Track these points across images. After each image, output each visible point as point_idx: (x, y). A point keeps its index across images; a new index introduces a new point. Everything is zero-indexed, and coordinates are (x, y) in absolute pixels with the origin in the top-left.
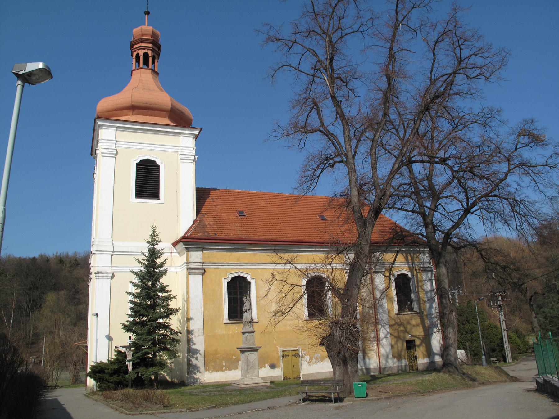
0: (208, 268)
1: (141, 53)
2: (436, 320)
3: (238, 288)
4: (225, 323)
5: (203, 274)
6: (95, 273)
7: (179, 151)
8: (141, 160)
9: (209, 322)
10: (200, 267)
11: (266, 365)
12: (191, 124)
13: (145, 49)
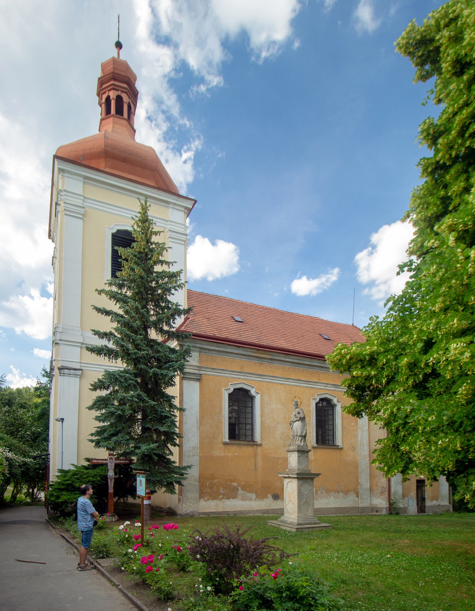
1: (113, 95)
3: (241, 399)
4: (225, 444)
5: (199, 380)
6: (59, 369)
7: (166, 226)
9: (206, 441)
11: (269, 495)
13: (118, 90)
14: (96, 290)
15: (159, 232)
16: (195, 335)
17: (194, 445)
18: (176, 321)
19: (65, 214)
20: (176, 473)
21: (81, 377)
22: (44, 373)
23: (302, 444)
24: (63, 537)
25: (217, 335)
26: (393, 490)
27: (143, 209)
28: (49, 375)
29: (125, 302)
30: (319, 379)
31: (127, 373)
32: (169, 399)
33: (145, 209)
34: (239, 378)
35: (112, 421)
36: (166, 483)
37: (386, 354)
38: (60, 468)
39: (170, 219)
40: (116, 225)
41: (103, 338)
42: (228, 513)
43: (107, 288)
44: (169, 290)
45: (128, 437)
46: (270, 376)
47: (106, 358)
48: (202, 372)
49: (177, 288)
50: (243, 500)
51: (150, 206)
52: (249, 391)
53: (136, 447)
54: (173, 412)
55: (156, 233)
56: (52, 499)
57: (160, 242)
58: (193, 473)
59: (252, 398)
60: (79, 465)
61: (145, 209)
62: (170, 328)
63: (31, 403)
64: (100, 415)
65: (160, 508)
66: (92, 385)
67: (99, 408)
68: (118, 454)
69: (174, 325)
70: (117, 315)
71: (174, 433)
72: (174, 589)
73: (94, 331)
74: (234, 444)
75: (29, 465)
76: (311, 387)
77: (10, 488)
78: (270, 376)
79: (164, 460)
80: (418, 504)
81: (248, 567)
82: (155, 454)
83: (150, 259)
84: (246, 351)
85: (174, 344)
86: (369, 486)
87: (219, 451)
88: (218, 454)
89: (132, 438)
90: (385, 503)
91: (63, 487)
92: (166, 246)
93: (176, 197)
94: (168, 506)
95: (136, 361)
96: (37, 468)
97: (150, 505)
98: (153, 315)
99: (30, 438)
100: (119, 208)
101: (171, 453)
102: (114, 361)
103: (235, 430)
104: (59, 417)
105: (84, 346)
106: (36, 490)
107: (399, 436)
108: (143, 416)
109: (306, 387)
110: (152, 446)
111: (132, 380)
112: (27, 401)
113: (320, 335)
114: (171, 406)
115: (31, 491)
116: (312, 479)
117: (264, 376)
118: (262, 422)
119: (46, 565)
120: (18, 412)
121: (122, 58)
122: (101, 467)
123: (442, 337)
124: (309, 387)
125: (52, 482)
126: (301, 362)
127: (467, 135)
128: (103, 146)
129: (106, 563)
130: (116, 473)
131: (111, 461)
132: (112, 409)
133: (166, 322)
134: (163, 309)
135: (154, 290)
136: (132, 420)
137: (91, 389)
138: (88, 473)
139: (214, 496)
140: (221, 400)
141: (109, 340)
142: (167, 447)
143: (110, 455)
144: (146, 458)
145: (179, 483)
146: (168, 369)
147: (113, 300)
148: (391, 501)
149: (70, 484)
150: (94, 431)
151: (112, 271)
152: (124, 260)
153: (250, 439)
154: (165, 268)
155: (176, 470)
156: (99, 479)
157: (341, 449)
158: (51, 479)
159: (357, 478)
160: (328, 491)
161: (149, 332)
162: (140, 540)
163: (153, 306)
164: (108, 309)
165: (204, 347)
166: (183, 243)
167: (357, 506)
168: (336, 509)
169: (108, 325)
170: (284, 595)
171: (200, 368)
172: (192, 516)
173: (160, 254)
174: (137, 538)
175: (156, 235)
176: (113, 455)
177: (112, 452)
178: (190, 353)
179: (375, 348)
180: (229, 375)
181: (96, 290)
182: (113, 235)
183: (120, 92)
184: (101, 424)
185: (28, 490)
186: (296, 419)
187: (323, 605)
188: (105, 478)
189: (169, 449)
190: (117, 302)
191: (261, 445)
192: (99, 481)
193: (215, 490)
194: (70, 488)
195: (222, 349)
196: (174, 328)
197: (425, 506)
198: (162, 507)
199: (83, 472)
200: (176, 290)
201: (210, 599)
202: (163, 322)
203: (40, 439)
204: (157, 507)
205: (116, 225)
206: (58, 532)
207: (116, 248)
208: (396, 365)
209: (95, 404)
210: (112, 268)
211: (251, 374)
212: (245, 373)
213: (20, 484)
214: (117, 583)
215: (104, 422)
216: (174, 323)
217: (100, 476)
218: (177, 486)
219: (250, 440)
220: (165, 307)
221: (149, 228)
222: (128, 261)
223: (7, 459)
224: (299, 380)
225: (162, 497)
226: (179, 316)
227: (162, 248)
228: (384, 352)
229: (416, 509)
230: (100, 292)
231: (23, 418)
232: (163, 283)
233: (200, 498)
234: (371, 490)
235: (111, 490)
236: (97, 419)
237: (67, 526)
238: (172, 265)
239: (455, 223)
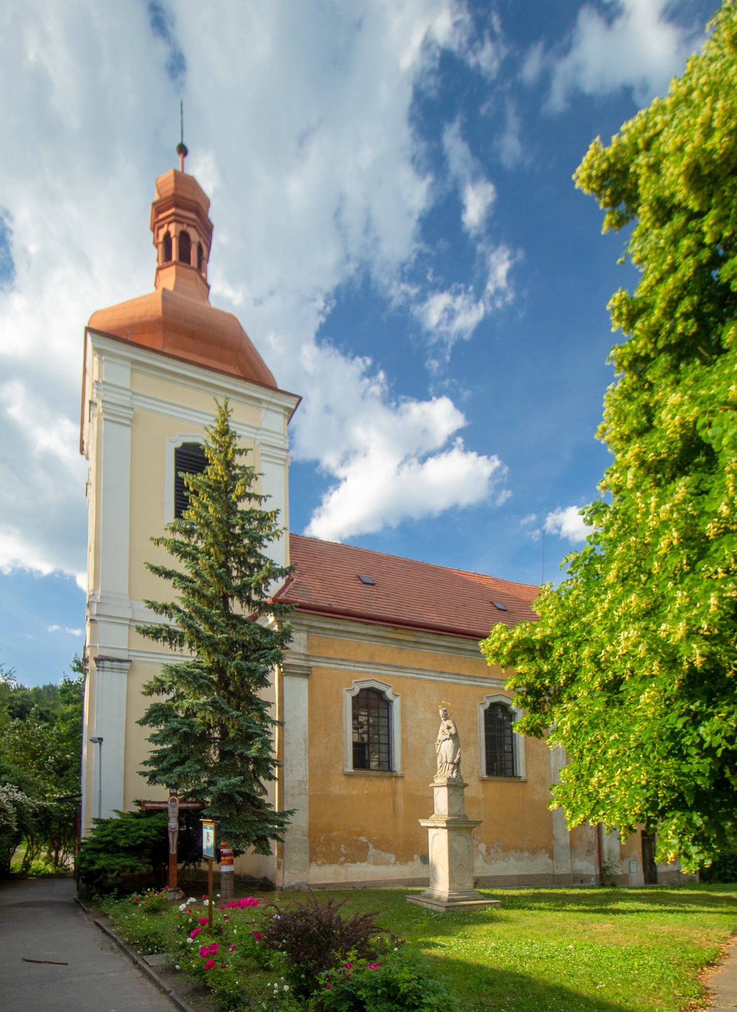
0: (317, 667)
3: (372, 704)
4: (348, 775)
5: (307, 676)
6: (97, 660)
7: (257, 437)
9: (319, 771)
11: (416, 857)
13: (182, 223)
14: (152, 539)
15: (246, 450)
16: (302, 607)
17: (300, 778)
18: (269, 588)
19: (105, 419)
20: (273, 822)
22: (75, 665)
23: (454, 775)
24: (98, 925)
25: (335, 606)
26: (605, 847)
27: (223, 415)
28: (81, 667)
29: (195, 559)
30: (489, 674)
31: (198, 667)
32: (260, 706)
33: (225, 415)
34: (368, 673)
35: (175, 742)
36: (255, 838)
37: (565, 639)
38: (97, 817)
39: (264, 426)
40: (182, 436)
41: (161, 613)
42: (352, 884)
43: (169, 535)
44: (259, 540)
45: (199, 767)
46: (414, 669)
47: (167, 644)
48: (312, 664)
49: (271, 537)
50: (376, 864)
51: (232, 410)
52: (384, 692)
53: (211, 783)
54: (267, 727)
55: (241, 452)
56: (83, 865)
57: (247, 466)
58: (299, 822)
59: (388, 703)
60: (126, 812)
61: (225, 415)
62: (262, 597)
63: (56, 712)
64: (157, 732)
65: (251, 878)
66: (145, 686)
67: (156, 723)
68: (185, 793)
69: (267, 594)
70: (182, 578)
71: (269, 760)
72: (243, 992)
73: (148, 602)
74: (361, 776)
75: (50, 812)
76: (477, 686)
77: (21, 851)
78: (414, 669)
79: (253, 803)
80: (644, 870)
81: (338, 955)
82: (238, 793)
83: (232, 491)
84: (378, 630)
85: (270, 621)
86: (568, 841)
87: (339, 788)
89: (206, 768)
91: (99, 846)
92: (256, 472)
93: (270, 392)
94: (262, 876)
95: (212, 646)
96: (65, 819)
97: (232, 873)
98: (237, 577)
99: (54, 769)
100: (189, 408)
101: (265, 791)
102: (178, 648)
103: (364, 755)
104: (96, 735)
105: (133, 624)
106: (61, 853)
107: (584, 762)
108: (221, 733)
109: (469, 685)
110: (235, 780)
111: (205, 678)
112: (49, 709)
113: (492, 603)
114: (263, 717)
115: (53, 854)
116: (470, 829)
117: (406, 668)
118: (404, 742)
119: (68, 967)
120: (35, 727)
122: (159, 814)
123: (619, 620)
124: (474, 686)
125: (84, 838)
126: (461, 646)
127: (677, 315)
128: (160, 313)
129: (156, 961)
130: (181, 824)
131: (173, 804)
132: (175, 725)
133: (255, 589)
134: (251, 567)
135: (238, 538)
136: (204, 739)
137: (143, 693)
138: (138, 824)
139: (332, 858)
141: (171, 616)
142: (258, 781)
143: (171, 794)
144: (225, 799)
145: (275, 837)
146: (258, 660)
147: (175, 554)
149: (110, 842)
150: (148, 757)
151: (176, 507)
152: (192, 493)
153: (387, 768)
154: (253, 505)
155: (271, 818)
156: (155, 832)
157: (525, 782)
158: (83, 835)
159: (551, 828)
160: (506, 849)
161: (231, 604)
162: (207, 925)
163: (237, 563)
164: (169, 568)
166: (282, 463)
167: (551, 872)
168: (519, 877)
169: (171, 593)
170: (379, 992)
171: (308, 657)
172: (298, 891)
173: (247, 484)
174: (203, 923)
175: (241, 454)
176: (176, 794)
177: (174, 791)
178: (290, 637)
179: (548, 631)
180: (352, 668)
181: (152, 539)
182: (177, 451)
184: (159, 747)
185: (49, 852)
186: (444, 737)
187: (430, 1005)
188: (164, 831)
189: (261, 785)
190: (181, 557)
191: (402, 777)
192: (154, 836)
193: (333, 849)
194: (110, 848)
195: (341, 628)
196: (267, 597)
197: (656, 873)
198: (254, 876)
199: (130, 822)
200: (270, 540)
201: (285, 1003)
202: (251, 588)
203: (68, 770)
204: (246, 877)
205: (182, 436)
206: (91, 917)
207: (181, 474)
208: (578, 656)
209: (148, 716)
210: (176, 503)
211: (386, 665)
212: (377, 664)
213: (37, 843)
214: (168, 989)
215: (162, 745)
216: (267, 590)
217: (156, 828)
218: (274, 844)
219: (387, 766)
220: (254, 565)
221: (230, 443)
222: (198, 495)
223: (15, 803)
224: (458, 674)
225: (249, 861)
226: (275, 578)
227: (249, 475)
228: (562, 636)
229: (643, 878)
230: (158, 542)
231: (42, 738)
232: (250, 529)
233: (311, 861)
234: (572, 846)
235: (173, 851)
236: (154, 739)
237: (104, 908)
238: (265, 500)
239: (643, 450)
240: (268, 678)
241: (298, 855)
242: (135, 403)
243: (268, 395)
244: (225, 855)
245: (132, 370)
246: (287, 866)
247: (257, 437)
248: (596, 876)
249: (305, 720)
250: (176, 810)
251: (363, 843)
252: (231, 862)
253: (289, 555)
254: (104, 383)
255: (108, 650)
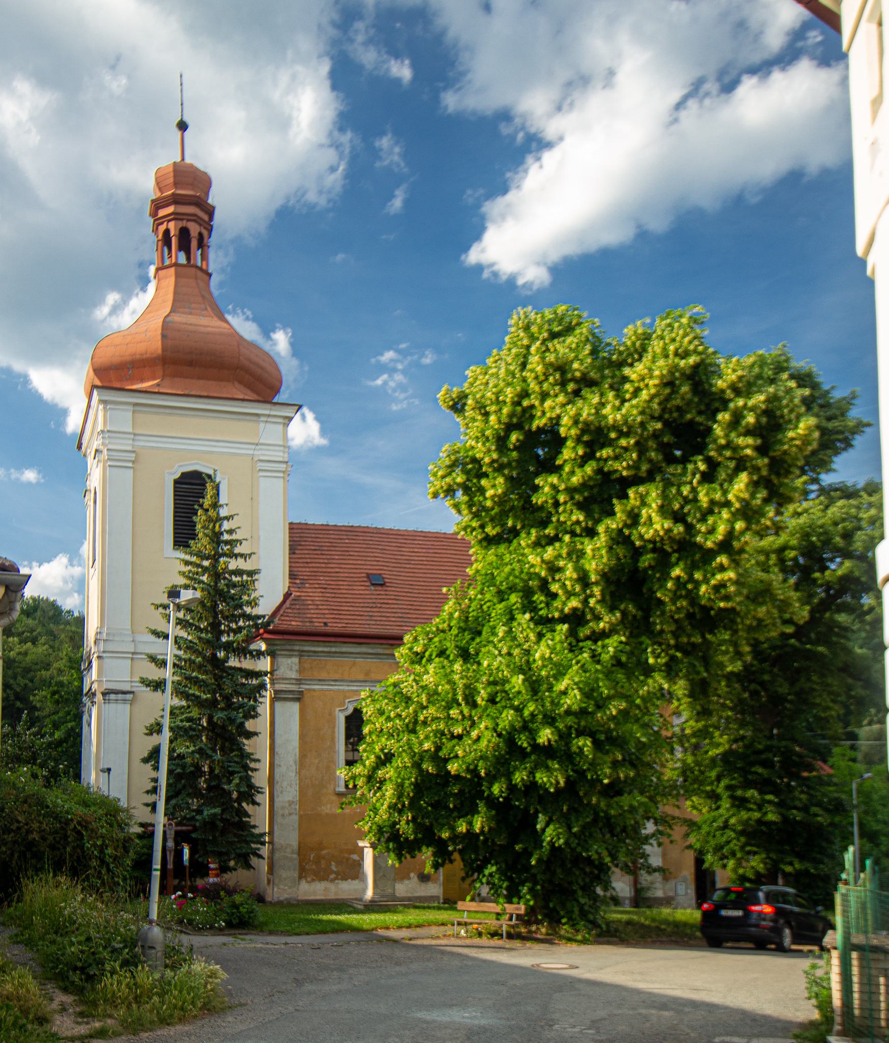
2: (613, 618)
5: (298, 700)
7: (256, 453)
8: (183, 474)
10: (294, 688)
11: (412, 875)
12: (276, 390)
13: (182, 220)
15: (232, 517)
17: (290, 799)
21: (132, 702)
39: (261, 441)
40: (180, 466)
84: (373, 648)
88: (328, 811)
90: (627, 889)
110: (218, 810)
121: (188, 160)
128: (160, 351)
137: (146, 734)
140: (334, 727)
148: (639, 886)
165: (306, 648)
166: (281, 475)
171: (299, 681)
180: (347, 688)
183: (185, 222)
195: (333, 649)
205: (180, 466)
233: (300, 878)
240: (259, 710)
241: (288, 873)
242: (137, 443)
243: (265, 409)
244: (213, 869)
245: (134, 412)
246: (276, 882)
247: (256, 453)
248: (630, 899)
249: (295, 743)
250: (173, 833)
251: (355, 861)
252: (217, 876)
253: (287, 565)
254: (108, 431)
255: (113, 683)
